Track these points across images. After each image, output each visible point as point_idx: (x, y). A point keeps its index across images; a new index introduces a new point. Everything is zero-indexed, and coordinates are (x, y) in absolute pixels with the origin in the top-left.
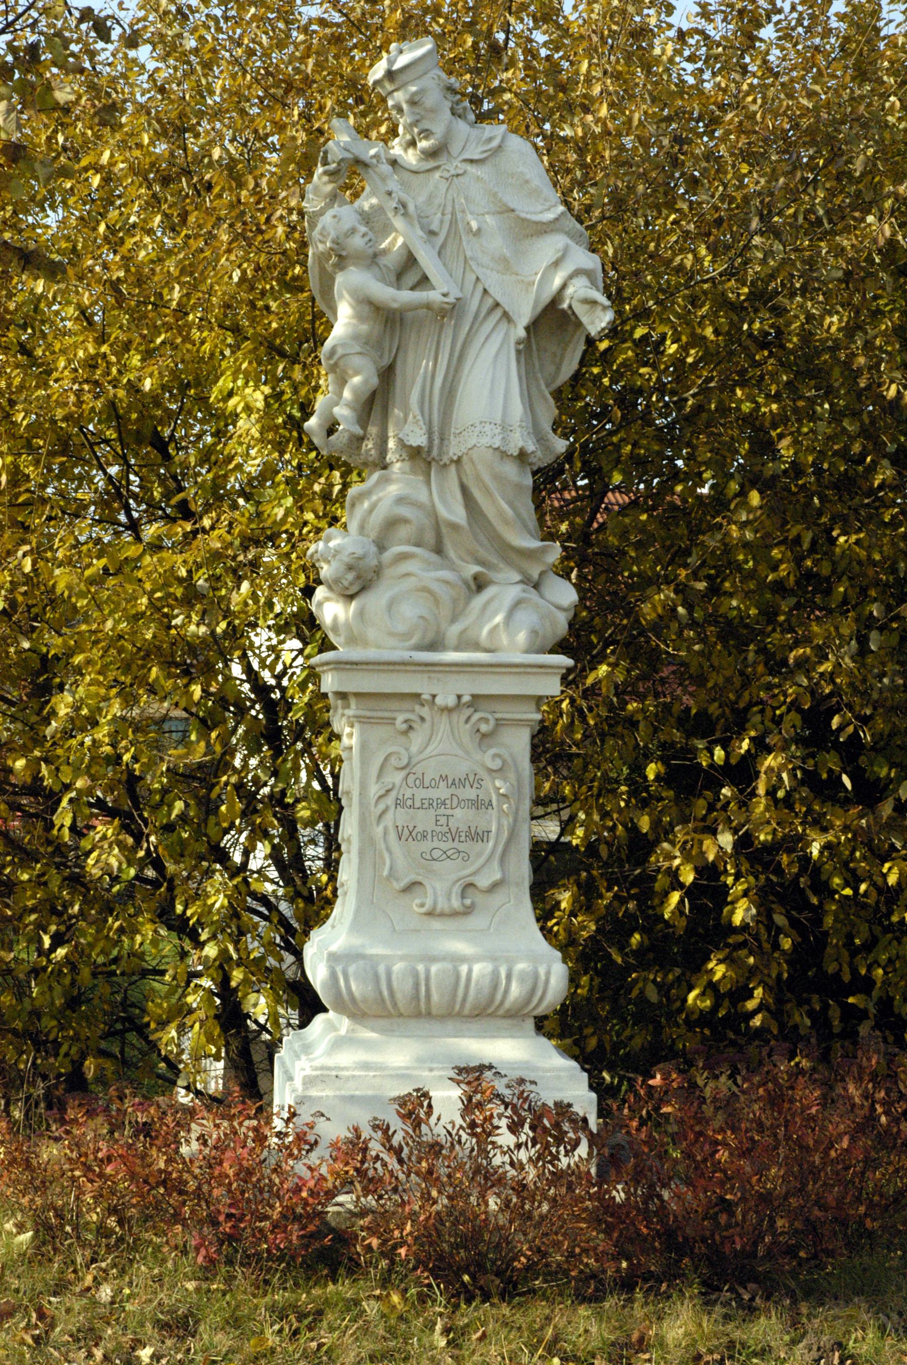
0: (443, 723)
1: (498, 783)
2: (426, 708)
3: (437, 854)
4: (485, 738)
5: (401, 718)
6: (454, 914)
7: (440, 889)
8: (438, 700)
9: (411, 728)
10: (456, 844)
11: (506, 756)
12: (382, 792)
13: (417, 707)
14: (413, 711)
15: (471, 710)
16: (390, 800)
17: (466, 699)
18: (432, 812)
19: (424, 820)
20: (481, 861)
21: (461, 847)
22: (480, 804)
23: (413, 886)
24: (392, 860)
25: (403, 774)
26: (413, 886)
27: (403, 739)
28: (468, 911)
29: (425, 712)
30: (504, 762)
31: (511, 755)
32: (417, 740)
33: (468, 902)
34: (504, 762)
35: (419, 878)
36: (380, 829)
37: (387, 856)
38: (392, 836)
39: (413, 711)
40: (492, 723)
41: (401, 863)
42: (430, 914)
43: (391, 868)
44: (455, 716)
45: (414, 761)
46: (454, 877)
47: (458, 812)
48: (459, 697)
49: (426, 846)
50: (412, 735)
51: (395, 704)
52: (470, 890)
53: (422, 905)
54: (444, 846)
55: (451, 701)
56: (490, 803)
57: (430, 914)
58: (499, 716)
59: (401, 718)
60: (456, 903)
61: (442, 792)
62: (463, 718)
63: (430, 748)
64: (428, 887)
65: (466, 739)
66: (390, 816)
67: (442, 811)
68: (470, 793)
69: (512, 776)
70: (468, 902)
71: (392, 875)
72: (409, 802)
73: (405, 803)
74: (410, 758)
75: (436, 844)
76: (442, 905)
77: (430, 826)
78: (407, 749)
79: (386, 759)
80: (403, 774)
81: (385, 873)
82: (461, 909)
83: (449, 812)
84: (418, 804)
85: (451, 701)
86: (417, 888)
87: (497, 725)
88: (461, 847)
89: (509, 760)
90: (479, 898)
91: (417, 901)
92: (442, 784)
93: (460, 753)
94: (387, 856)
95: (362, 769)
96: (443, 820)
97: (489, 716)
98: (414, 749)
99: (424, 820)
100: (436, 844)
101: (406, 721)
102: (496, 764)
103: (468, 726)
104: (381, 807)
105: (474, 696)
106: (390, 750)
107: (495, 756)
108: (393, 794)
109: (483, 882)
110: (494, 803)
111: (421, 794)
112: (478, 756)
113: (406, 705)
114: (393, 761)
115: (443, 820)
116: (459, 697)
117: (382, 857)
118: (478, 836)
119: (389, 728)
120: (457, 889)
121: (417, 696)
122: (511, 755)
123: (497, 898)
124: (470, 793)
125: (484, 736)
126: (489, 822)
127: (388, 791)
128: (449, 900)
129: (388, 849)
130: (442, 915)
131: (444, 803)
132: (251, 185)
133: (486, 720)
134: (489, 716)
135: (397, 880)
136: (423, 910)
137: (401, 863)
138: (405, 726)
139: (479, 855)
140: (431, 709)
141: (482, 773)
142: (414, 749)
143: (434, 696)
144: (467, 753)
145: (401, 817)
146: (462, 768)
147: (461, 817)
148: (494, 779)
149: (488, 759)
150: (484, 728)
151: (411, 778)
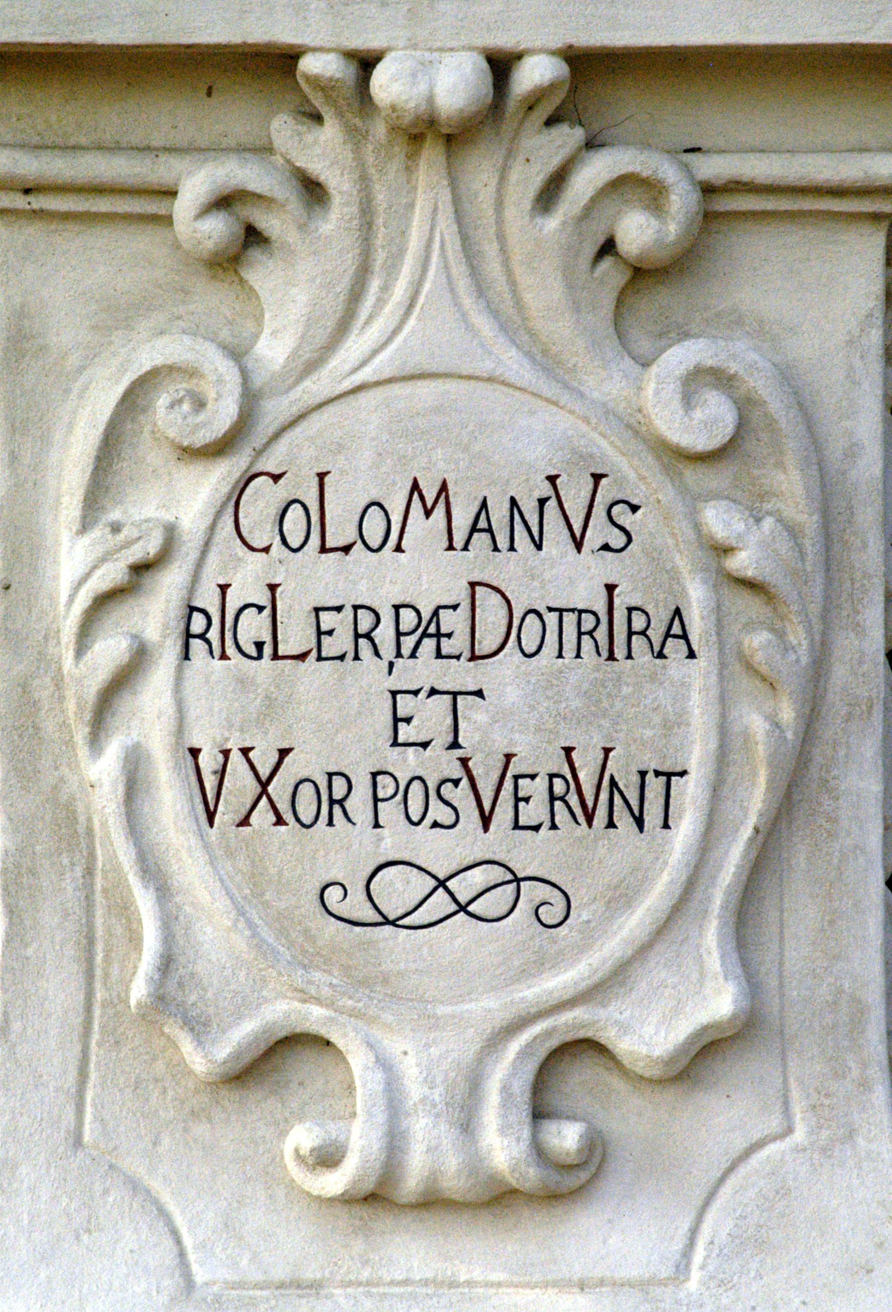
0: (422, 203)
1: (720, 520)
2: (330, 132)
3: (398, 890)
4: (643, 288)
5: (196, 184)
6: (498, 1199)
7: (421, 1062)
8: (386, 83)
9: (253, 236)
10: (499, 840)
11: (761, 384)
12: (113, 573)
13: (283, 129)
14: (265, 149)
15: (569, 136)
16: (154, 617)
17: (536, 73)
18: (370, 675)
19: (333, 718)
20: (635, 922)
21: (530, 854)
22: (611, 631)
23: (278, 1057)
24: (168, 937)
25: (218, 477)
26: (278, 1057)
27: (212, 299)
28: (565, 1185)
29: (322, 149)
30: (746, 408)
31: (787, 376)
32: (287, 298)
33: (566, 1137)
34: (746, 408)
35: (314, 1017)
36: (104, 770)
37: (144, 902)
38: (170, 800)
39: (265, 149)
40: (681, 201)
41: (217, 935)
42: (375, 1198)
43: (167, 963)
44: (481, 171)
45: (276, 410)
46: (489, 1007)
47: (505, 676)
48: (501, 65)
49: (342, 851)
50: (262, 274)
51: (164, 115)
52: (580, 1076)
53: (327, 1158)
54: (440, 850)
55: (455, 83)
56: (677, 624)
57: (375, 1198)
58: (713, 168)
59: (196, 184)
60: (502, 1147)
61: (424, 573)
62: (528, 178)
63: (355, 346)
64: (358, 1060)
65: (543, 292)
66: (154, 693)
67: (424, 670)
68: (569, 577)
69: (791, 485)
70: (566, 1137)
71: (173, 998)
72: (253, 627)
73: (229, 627)
74: (250, 401)
75: (395, 838)
76: (433, 1150)
77: (361, 747)
78: (237, 354)
79: (134, 399)
80: (218, 477)
81: (139, 990)
82: (531, 1176)
83: (459, 675)
84: (296, 635)
85: (455, 83)
86: (304, 1066)
87: (710, 219)
88: (530, 854)
89: (776, 404)
90: (630, 1118)
91: (303, 1137)
92: (423, 530)
93: (512, 362)
94: (144, 902)
95: (94, 848)
96: (430, 718)
97: (668, 171)
98: (273, 350)
99: (333, 718)
100: (395, 838)
101: (224, 202)
102: (707, 423)
103: (552, 223)
104: (110, 649)
105: (588, 66)
106: (148, 356)
107: (699, 380)
108: (170, 584)
109: (648, 1031)
110: (697, 624)
111: (313, 581)
112: (607, 381)
113: (234, 114)
114: (165, 414)
115: (430, 718)
116: (501, 65)
117: (124, 909)
118: (610, 798)
119: (142, 242)
120: (508, 1072)
121: (275, 65)
122: (787, 376)
123: (725, 1116)
124: (569, 577)
125: (643, 275)
126: (674, 724)
127: (142, 569)
128: (467, 1125)
129: (152, 871)
130: (432, 1202)
131: (432, 630)
132: (855, 1073)
133: (644, 190)
134: (668, 171)
135: (199, 1027)
136: (334, 1183)
137: (217, 935)
138: (216, 229)
139: (621, 898)
140: (356, 136)
141: (633, 474)
142: (273, 350)
143: (366, 63)
144: (546, 360)
145: (213, 700)
146: (521, 442)
147: (520, 708)
148: (694, 501)
149: (664, 394)
150: (637, 231)
151: (261, 501)
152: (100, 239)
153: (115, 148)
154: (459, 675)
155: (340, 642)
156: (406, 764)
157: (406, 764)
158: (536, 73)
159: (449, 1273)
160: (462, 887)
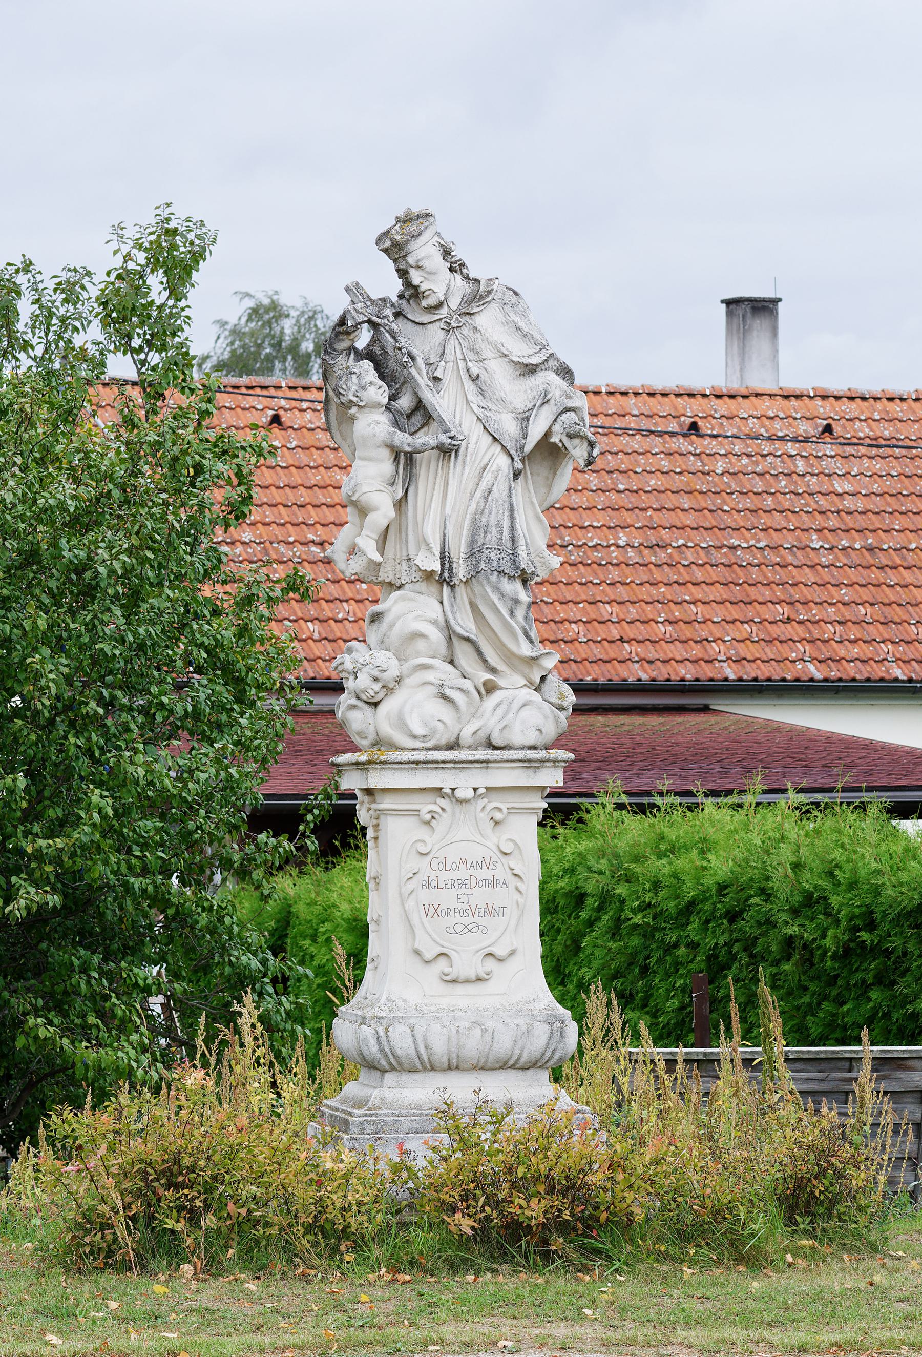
3: (459, 928)
10: (476, 919)
22: (493, 883)
49: (451, 920)
61: (463, 874)
62: (479, 807)
67: (462, 890)
77: (453, 904)
83: (468, 891)
84: (441, 885)
92: (463, 867)
111: (444, 875)
115: (464, 898)
118: (492, 911)
145: (425, 896)
147: (480, 897)
151: (435, 863)
152: (407, 818)
153: (369, 762)
154: (468, 891)
155: (449, 886)
156: (460, 906)
157: (460, 906)
158: (482, 791)
159: (729, 1082)
160: (470, 927)
